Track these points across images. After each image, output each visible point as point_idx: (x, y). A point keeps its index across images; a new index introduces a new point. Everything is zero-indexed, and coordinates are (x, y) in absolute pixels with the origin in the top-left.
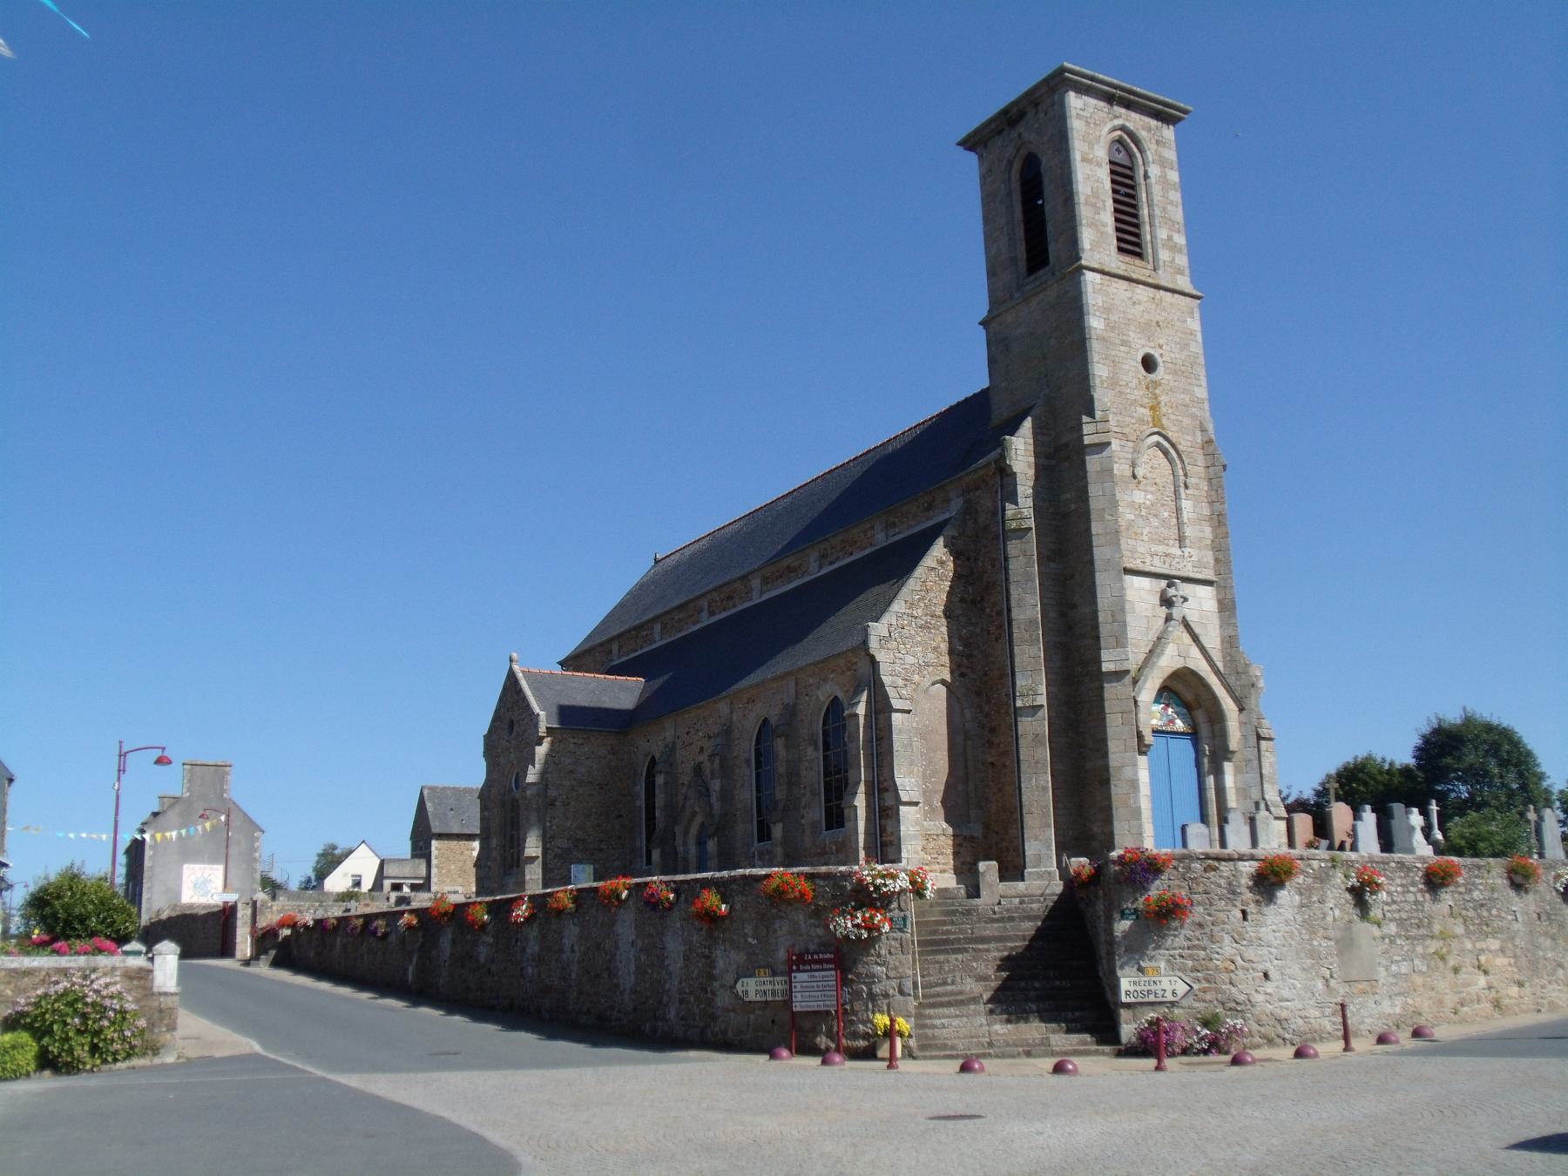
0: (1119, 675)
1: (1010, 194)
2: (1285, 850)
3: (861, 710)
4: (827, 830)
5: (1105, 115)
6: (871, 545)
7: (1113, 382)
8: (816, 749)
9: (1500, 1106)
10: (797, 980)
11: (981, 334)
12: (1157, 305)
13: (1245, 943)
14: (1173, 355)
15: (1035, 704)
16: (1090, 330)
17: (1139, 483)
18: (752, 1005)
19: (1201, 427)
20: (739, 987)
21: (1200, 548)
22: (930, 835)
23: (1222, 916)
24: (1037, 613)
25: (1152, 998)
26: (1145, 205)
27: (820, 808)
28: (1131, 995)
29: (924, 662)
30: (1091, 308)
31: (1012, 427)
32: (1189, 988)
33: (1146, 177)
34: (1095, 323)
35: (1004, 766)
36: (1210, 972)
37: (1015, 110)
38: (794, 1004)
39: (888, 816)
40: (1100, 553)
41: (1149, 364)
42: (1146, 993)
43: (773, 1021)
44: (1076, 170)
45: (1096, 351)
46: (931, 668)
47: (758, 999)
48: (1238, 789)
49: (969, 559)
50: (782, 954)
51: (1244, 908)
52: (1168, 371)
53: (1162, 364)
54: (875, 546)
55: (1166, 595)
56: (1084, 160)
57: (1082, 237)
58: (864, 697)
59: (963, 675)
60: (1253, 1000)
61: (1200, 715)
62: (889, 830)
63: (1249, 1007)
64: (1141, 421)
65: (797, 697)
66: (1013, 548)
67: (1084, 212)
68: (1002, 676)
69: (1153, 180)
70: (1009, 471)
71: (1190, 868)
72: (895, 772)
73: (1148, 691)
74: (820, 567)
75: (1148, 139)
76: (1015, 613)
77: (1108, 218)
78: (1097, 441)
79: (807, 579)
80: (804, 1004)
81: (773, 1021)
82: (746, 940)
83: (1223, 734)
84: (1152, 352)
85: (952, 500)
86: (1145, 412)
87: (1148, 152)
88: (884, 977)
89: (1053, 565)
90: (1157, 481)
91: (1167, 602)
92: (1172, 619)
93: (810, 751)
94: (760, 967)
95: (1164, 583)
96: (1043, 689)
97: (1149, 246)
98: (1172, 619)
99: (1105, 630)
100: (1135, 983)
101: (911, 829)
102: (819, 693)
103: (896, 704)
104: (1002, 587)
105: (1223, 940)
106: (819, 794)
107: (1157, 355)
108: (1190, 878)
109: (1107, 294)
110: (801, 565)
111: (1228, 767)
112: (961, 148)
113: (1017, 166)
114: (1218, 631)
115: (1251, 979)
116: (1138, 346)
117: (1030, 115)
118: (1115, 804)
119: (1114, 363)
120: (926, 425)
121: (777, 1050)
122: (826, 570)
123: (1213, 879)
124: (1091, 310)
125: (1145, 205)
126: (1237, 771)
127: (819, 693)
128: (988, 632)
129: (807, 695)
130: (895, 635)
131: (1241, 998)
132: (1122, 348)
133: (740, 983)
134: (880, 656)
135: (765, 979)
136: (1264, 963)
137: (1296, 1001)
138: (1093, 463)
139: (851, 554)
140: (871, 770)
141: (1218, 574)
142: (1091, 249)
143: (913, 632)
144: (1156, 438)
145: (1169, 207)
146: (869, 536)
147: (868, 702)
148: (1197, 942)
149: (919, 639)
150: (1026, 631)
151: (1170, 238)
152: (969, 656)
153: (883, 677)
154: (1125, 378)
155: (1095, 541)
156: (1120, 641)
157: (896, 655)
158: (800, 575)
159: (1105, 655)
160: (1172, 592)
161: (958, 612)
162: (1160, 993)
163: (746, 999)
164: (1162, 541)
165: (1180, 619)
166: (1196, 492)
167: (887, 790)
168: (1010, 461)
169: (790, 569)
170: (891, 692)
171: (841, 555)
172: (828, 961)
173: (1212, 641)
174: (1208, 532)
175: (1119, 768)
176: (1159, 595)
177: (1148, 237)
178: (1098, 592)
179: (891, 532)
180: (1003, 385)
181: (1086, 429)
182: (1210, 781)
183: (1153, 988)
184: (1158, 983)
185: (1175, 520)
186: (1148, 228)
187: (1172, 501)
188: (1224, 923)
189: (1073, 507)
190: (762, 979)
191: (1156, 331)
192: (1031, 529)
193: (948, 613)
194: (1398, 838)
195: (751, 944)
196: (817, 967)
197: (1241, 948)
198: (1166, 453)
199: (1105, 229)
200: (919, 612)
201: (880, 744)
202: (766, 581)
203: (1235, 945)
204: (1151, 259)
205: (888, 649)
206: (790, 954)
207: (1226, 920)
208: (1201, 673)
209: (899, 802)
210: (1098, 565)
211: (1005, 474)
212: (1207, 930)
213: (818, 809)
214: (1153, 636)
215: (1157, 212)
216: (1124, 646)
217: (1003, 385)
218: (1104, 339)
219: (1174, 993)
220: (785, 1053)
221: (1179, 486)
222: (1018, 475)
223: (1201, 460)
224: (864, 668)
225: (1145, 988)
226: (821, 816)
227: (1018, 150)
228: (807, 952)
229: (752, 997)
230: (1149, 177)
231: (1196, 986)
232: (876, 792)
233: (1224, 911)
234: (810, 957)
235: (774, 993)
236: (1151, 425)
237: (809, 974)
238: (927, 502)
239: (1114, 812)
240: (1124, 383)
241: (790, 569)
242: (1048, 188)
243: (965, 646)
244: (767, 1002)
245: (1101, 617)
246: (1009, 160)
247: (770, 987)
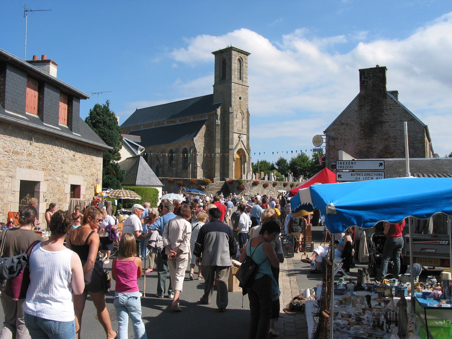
0: (232, 149)
2: (255, 180)
7: (235, 101)
9: (429, 170)
34: (233, 92)
40: (230, 130)
41: (240, 98)
45: (233, 96)
48: (247, 167)
56: (234, 63)
59: (207, 146)
66: (217, 127)
73: (235, 152)
74: (179, 122)
76: (216, 138)
91: (239, 137)
95: (239, 135)
99: (230, 142)
103: (197, 151)
111: (246, 164)
117: (225, 52)
118: (229, 169)
126: (247, 164)
134: (195, 143)
138: (231, 115)
141: (247, 133)
151: (245, 76)
156: (232, 144)
159: (230, 146)
173: (245, 144)
175: (230, 164)
181: (230, 109)
192: (290, 206)
193: (205, 136)
194: (270, 179)
198: (241, 113)
202: (167, 122)
211: (216, 114)
214: (237, 143)
224: (192, 145)
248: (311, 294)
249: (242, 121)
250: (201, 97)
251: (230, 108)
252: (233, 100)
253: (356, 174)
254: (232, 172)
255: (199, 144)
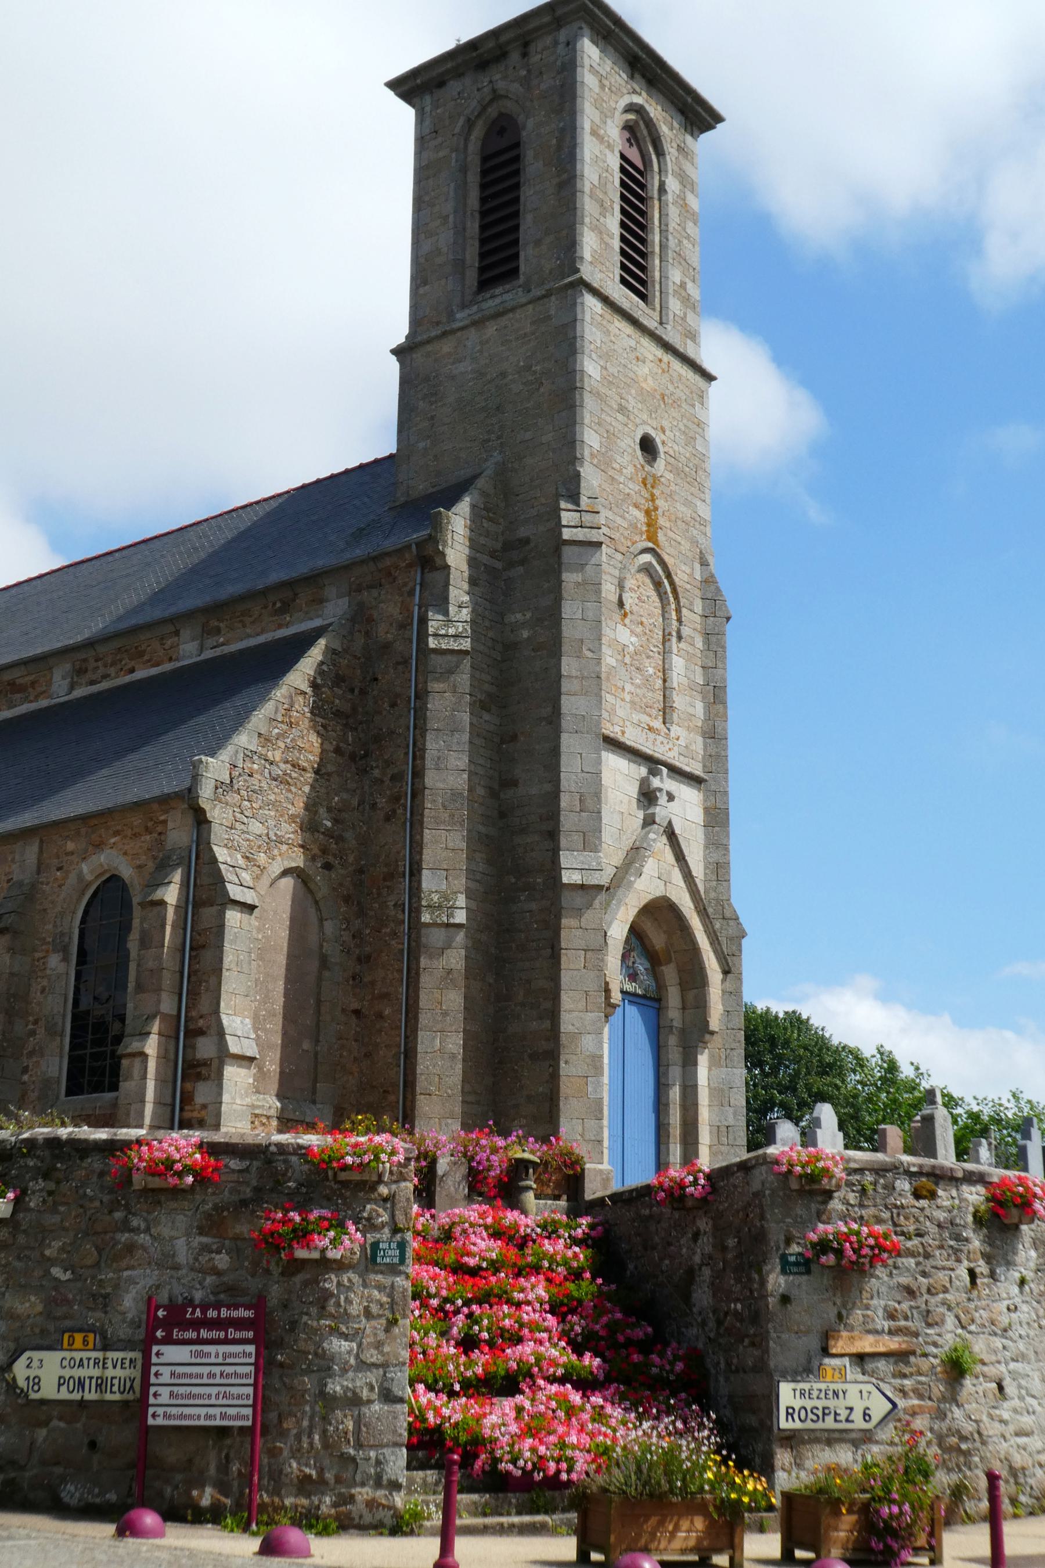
1: (464, 170)
3: (171, 894)
4: (69, 1093)
5: (624, 83)
6: (171, 659)
8: (66, 959)
10: (162, 1360)
11: (393, 367)
12: (663, 371)
13: (973, 1328)
14: (676, 448)
15: (452, 921)
16: (583, 376)
17: (625, 615)
18: (44, 1408)
19: (701, 558)
20: (20, 1370)
21: (688, 728)
22: (257, 1116)
23: (942, 1277)
24: (460, 782)
25: (829, 1423)
26: (657, 230)
27: (61, 1057)
28: (796, 1416)
29: (276, 834)
30: (586, 344)
31: (450, 499)
32: (890, 1406)
33: (662, 189)
34: (591, 368)
35: (380, 1016)
36: (923, 1379)
37: (491, 44)
38: (151, 1410)
39: (199, 1077)
40: (571, 705)
41: (647, 446)
42: (820, 1414)
43: (93, 1445)
44: (582, 143)
45: (590, 409)
46: (284, 847)
47: (64, 1395)
49: (352, 690)
50: (130, 1302)
51: (972, 1265)
52: (669, 468)
53: (662, 455)
54: (177, 659)
55: (649, 785)
57: (581, 241)
58: (177, 876)
60: (985, 1433)
61: (670, 972)
62: (199, 1099)
63: (978, 1444)
64: (634, 526)
65: (39, 872)
67: (588, 206)
68: (390, 876)
69: (670, 197)
70: (438, 562)
71: (894, 1188)
72: (222, 1004)
74: (72, 687)
75: (669, 140)
76: (431, 778)
77: (613, 223)
78: (581, 538)
79: (44, 703)
80: (174, 1411)
81: (93, 1445)
82: (47, 1273)
83: (701, 1005)
84: (653, 433)
85: (327, 601)
86: (641, 516)
87: (668, 158)
88: (352, 1361)
89: (486, 716)
90: (644, 620)
91: (648, 797)
92: (654, 822)
93: (54, 961)
94: (73, 1330)
96: (461, 901)
97: (657, 287)
98: (654, 822)
99: (568, 821)
100: (802, 1394)
101: (238, 1101)
102: (85, 868)
104: (406, 739)
105: (943, 1321)
106: (62, 1035)
107: (658, 441)
108: (896, 1207)
109: (608, 332)
110: (33, 684)
111: (703, 1060)
112: (391, 94)
113: (478, 132)
114: (701, 853)
115: (981, 1394)
116: (638, 421)
117: (515, 57)
119: (610, 437)
120: (267, 507)
121: (133, 1514)
122: (79, 693)
123: (927, 1212)
124: (588, 348)
125: (657, 230)
126: (714, 1063)
127: (85, 868)
128: (374, 806)
129: (59, 869)
130: (239, 784)
131: (968, 1427)
132: (620, 417)
133: (22, 1362)
134: (217, 814)
135: (85, 1355)
136: (997, 1365)
137: (1036, 1437)
139: (132, 671)
140: (176, 998)
142: (591, 263)
143: (264, 784)
144: (647, 558)
145: (685, 242)
146: (166, 647)
147: (185, 884)
148: (903, 1323)
149: (272, 797)
150: (445, 807)
151: (683, 285)
152: (340, 839)
153: (215, 848)
154: (619, 459)
155: (565, 686)
156: (591, 841)
157: (238, 815)
158: (32, 698)
159: (566, 859)
160: (656, 782)
161: (330, 768)
162: (843, 1414)
163: (33, 1396)
164: (645, 708)
165: (665, 824)
166: (690, 649)
167: (201, 1032)
168: (444, 546)
169: (21, 689)
170: (228, 874)
171: (112, 671)
172: (239, 1324)
174: (699, 708)
176: (637, 784)
177: (657, 274)
178: (562, 762)
179: (210, 642)
180: (421, 445)
181: (567, 517)
182: (675, 1073)
183: (831, 1403)
184: (841, 1394)
185: (660, 682)
186: (657, 262)
187: (659, 653)
188: (946, 1290)
189: (525, 634)
190: (78, 1355)
191: (659, 405)
195: (56, 1279)
196: (214, 1334)
197: (968, 1336)
198: (658, 585)
199: (610, 241)
200: (278, 756)
201: (196, 957)
203: (960, 1331)
204: (658, 306)
205: (227, 804)
206: (151, 1305)
207: (948, 1285)
208: (683, 909)
209: (224, 1055)
210: (567, 722)
212: (921, 1302)
213: (57, 1059)
215: (672, 243)
216: (596, 849)
217: (421, 445)
218: (597, 395)
219: (866, 1416)
220: (150, 1519)
221: (670, 634)
222: (452, 570)
223: (698, 605)
225: (820, 1404)
226: (61, 1068)
227: (484, 108)
228: (190, 1302)
229: (49, 1391)
230: (665, 191)
231: (901, 1403)
232: (182, 1034)
233: (944, 1268)
234: (198, 1313)
235: (101, 1384)
236: (644, 537)
237: (194, 1348)
238: (281, 600)
239: (561, 1104)
240: (617, 467)
241: (21, 689)
242: (533, 165)
243: (336, 821)
244: (82, 1403)
245: (565, 801)
246: (469, 120)
247: (96, 1372)
248: (396, 1531)
249: (665, 653)
250: (279, 495)
251: (563, 505)
252: (591, 438)
253: (89, 1359)
254: (591, 1123)
255: (256, 827)
